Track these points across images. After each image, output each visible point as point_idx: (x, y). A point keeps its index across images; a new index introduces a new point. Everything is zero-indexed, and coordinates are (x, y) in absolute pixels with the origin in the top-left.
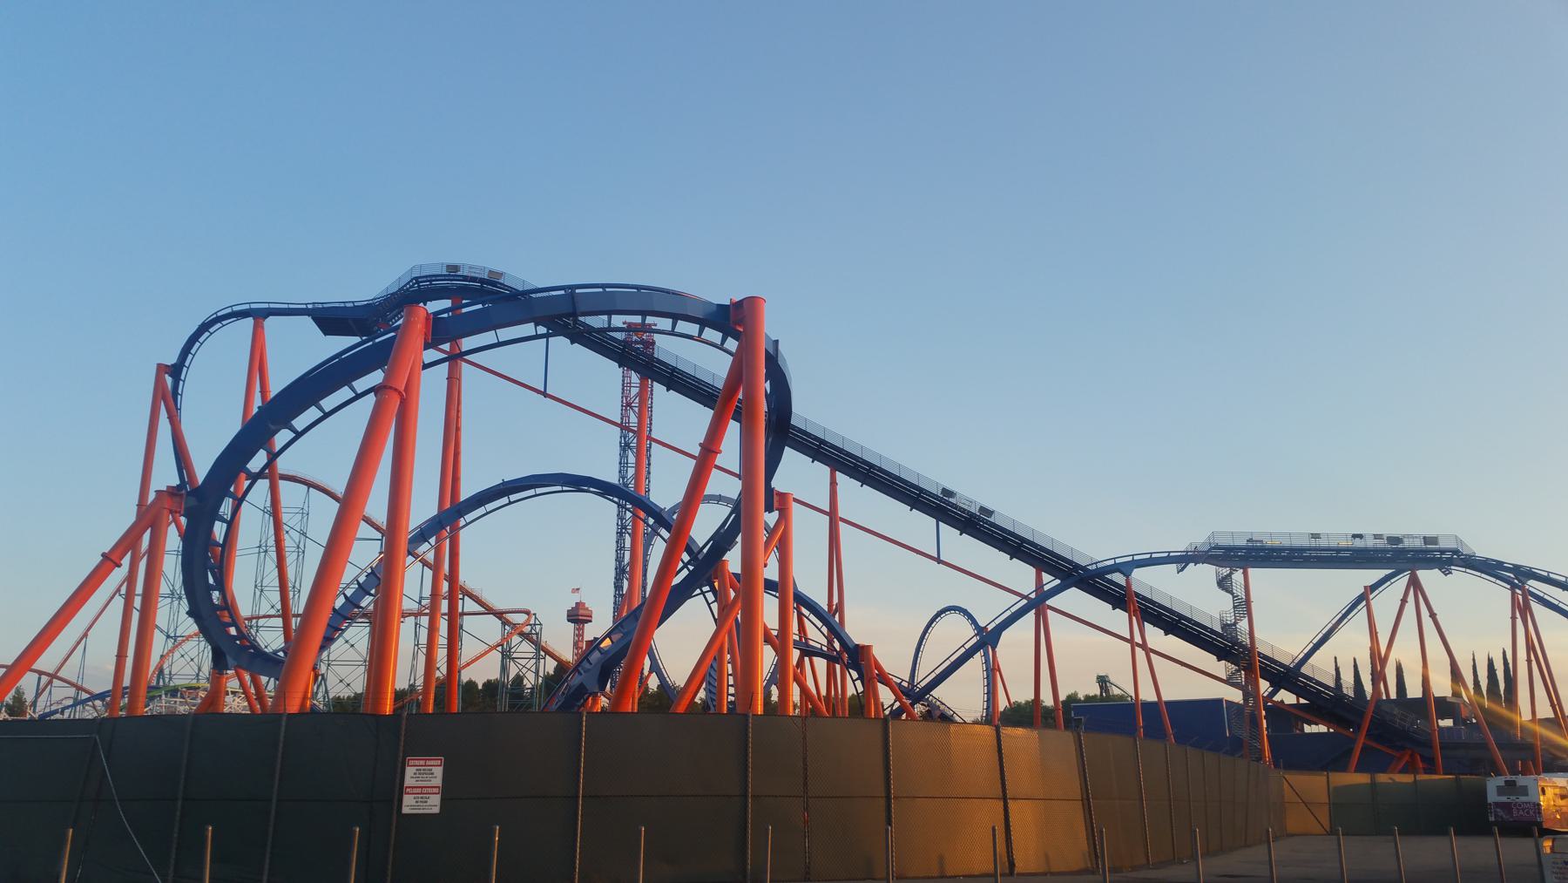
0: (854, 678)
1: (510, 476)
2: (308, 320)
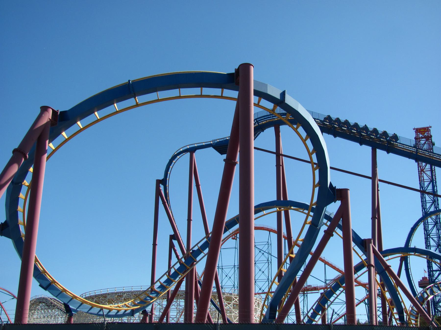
0: (160, 280)
1: (412, 226)
2: (211, 149)
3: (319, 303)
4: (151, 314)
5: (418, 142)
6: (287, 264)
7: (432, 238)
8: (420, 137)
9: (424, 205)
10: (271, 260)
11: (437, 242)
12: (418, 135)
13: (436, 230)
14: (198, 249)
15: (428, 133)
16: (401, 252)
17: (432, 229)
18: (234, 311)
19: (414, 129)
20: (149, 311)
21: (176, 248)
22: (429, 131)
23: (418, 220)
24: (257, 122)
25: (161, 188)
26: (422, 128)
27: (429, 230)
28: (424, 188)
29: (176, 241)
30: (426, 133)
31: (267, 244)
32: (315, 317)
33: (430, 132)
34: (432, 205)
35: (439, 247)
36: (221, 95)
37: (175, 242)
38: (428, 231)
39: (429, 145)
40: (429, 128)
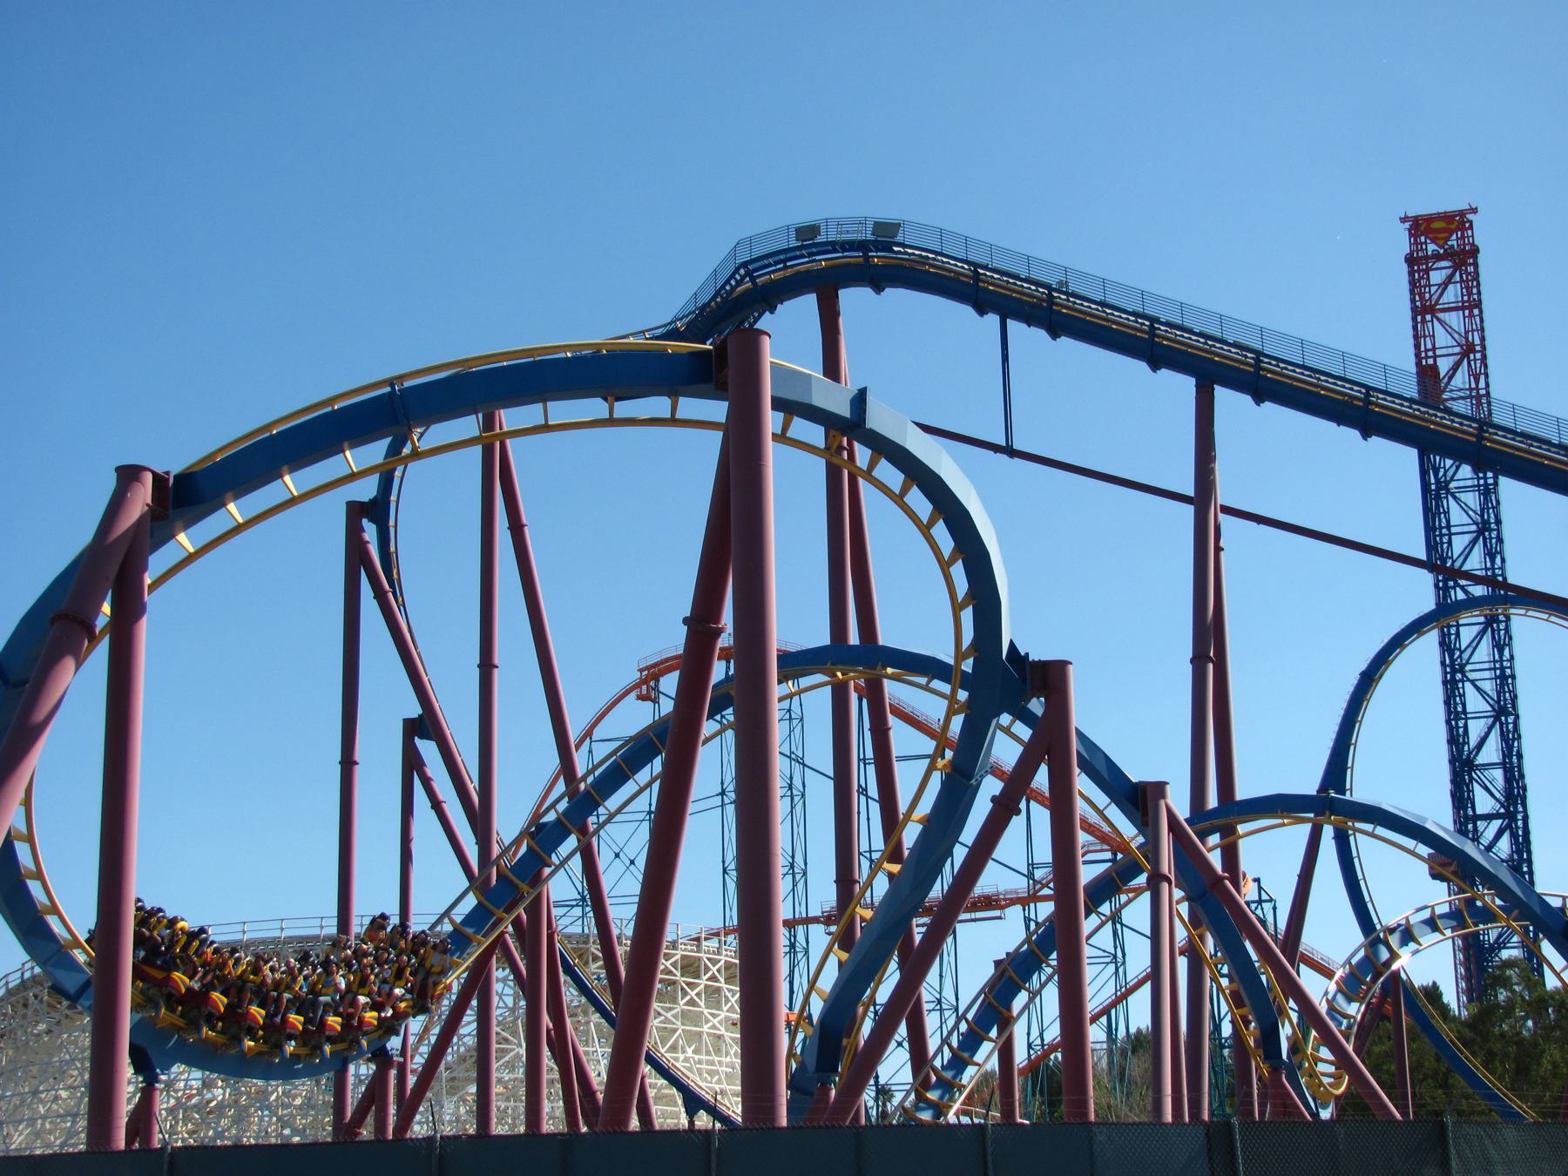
3: (990, 996)
4: (401, 1060)
5: (1419, 274)
6: (869, 800)
7: (1473, 682)
8: (1429, 253)
9: (1442, 543)
10: (804, 786)
11: (1496, 699)
12: (1421, 244)
13: (1488, 648)
14: (558, 820)
15: (1463, 237)
16: (1282, 812)
17: (1474, 644)
18: (662, 1011)
19: (1404, 220)
20: (397, 1050)
21: (429, 771)
22: (1467, 229)
23: (1386, 641)
24: (748, 273)
25: (367, 536)
26: (1438, 213)
27: (1463, 648)
28: (1442, 470)
29: (433, 744)
30: (1454, 237)
31: (787, 716)
32: (974, 1049)
33: (1470, 232)
34: (1474, 542)
35: (1503, 718)
36: (669, 416)
37: (428, 749)
38: (1457, 654)
39: (1467, 288)
40: (1467, 216)
